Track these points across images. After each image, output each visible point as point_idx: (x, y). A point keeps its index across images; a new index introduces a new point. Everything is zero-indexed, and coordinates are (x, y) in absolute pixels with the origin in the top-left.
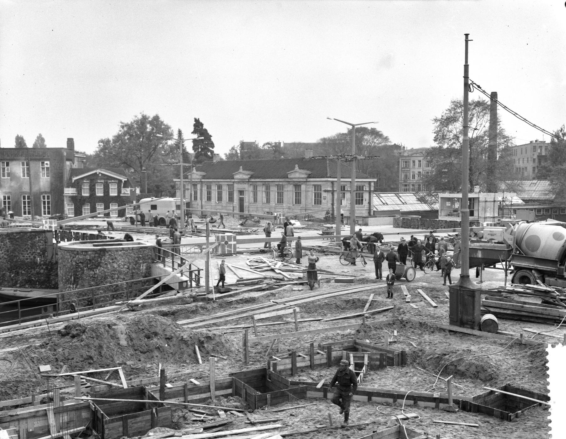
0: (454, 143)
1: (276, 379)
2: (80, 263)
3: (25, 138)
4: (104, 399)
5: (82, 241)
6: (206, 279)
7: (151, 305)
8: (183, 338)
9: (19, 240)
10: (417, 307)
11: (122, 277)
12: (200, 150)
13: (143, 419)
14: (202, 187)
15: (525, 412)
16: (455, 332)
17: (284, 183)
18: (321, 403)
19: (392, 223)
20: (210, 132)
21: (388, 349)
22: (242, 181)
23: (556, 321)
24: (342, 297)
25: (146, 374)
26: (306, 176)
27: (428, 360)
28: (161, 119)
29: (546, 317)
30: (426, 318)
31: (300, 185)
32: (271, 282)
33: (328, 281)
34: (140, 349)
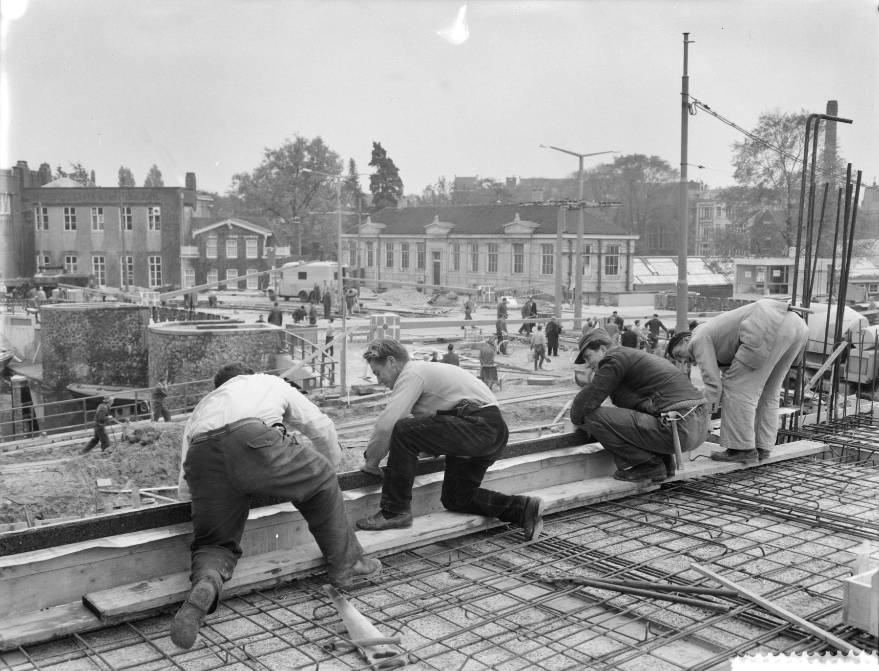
2: (178, 351)
6: (341, 376)
9: (103, 320)
12: (381, 190)
14: (379, 246)
17: (499, 242)
20: (397, 163)
22: (438, 238)
28: (325, 143)
31: (522, 245)
33: (519, 382)
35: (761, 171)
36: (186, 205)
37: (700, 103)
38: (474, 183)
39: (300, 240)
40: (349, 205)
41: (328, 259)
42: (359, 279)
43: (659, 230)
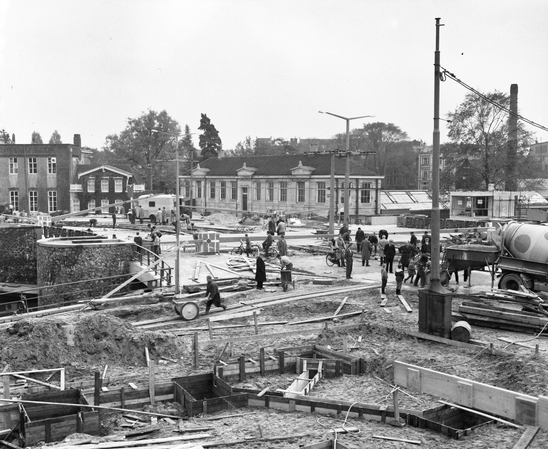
0: (470, 138)
1: (221, 385)
2: (57, 259)
3: (41, 135)
4: (29, 402)
5: (62, 238)
6: (176, 278)
7: (114, 304)
8: (133, 340)
9: (8, 236)
10: (390, 312)
11: (99, 274)
12: (207, 146)
13: (70, 422)
14: (206, 184)
15: (476, 431)
16: (424, 340)
17: (287, 180)
18: (262, 413)
19: (396, 222)
20: (217, 128)
21: (347, 356)
22: (245, 178)
23: (536, 330)
24: (314, 299)
25: (89, 376)
26: (310, 173)
27: (387, 369)
28: (169, 115)
29: (526, 325)
30: (397, 323)
31: (304, 182)
32: (246, 282)
33: (307, 282)
34: (88, 350)
35: (466, 132)
36: (74, 156)
37: (448, 72)
38: (269, 142)
39: (152, 179)
40: (185, 157)
41: (171, 193)
42: (191, 207)
43: (394, 173)
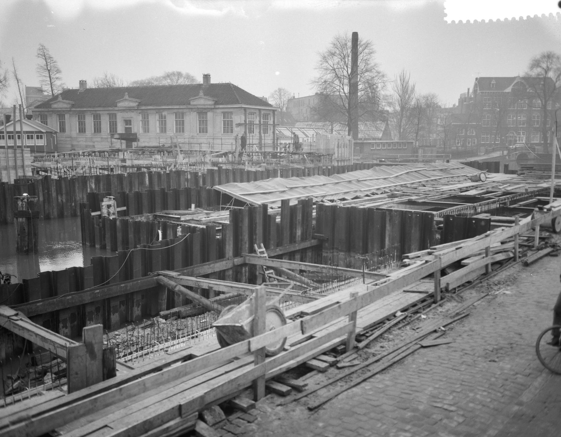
31: (206, 113)
